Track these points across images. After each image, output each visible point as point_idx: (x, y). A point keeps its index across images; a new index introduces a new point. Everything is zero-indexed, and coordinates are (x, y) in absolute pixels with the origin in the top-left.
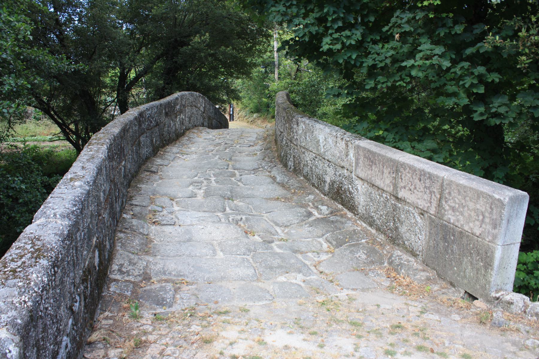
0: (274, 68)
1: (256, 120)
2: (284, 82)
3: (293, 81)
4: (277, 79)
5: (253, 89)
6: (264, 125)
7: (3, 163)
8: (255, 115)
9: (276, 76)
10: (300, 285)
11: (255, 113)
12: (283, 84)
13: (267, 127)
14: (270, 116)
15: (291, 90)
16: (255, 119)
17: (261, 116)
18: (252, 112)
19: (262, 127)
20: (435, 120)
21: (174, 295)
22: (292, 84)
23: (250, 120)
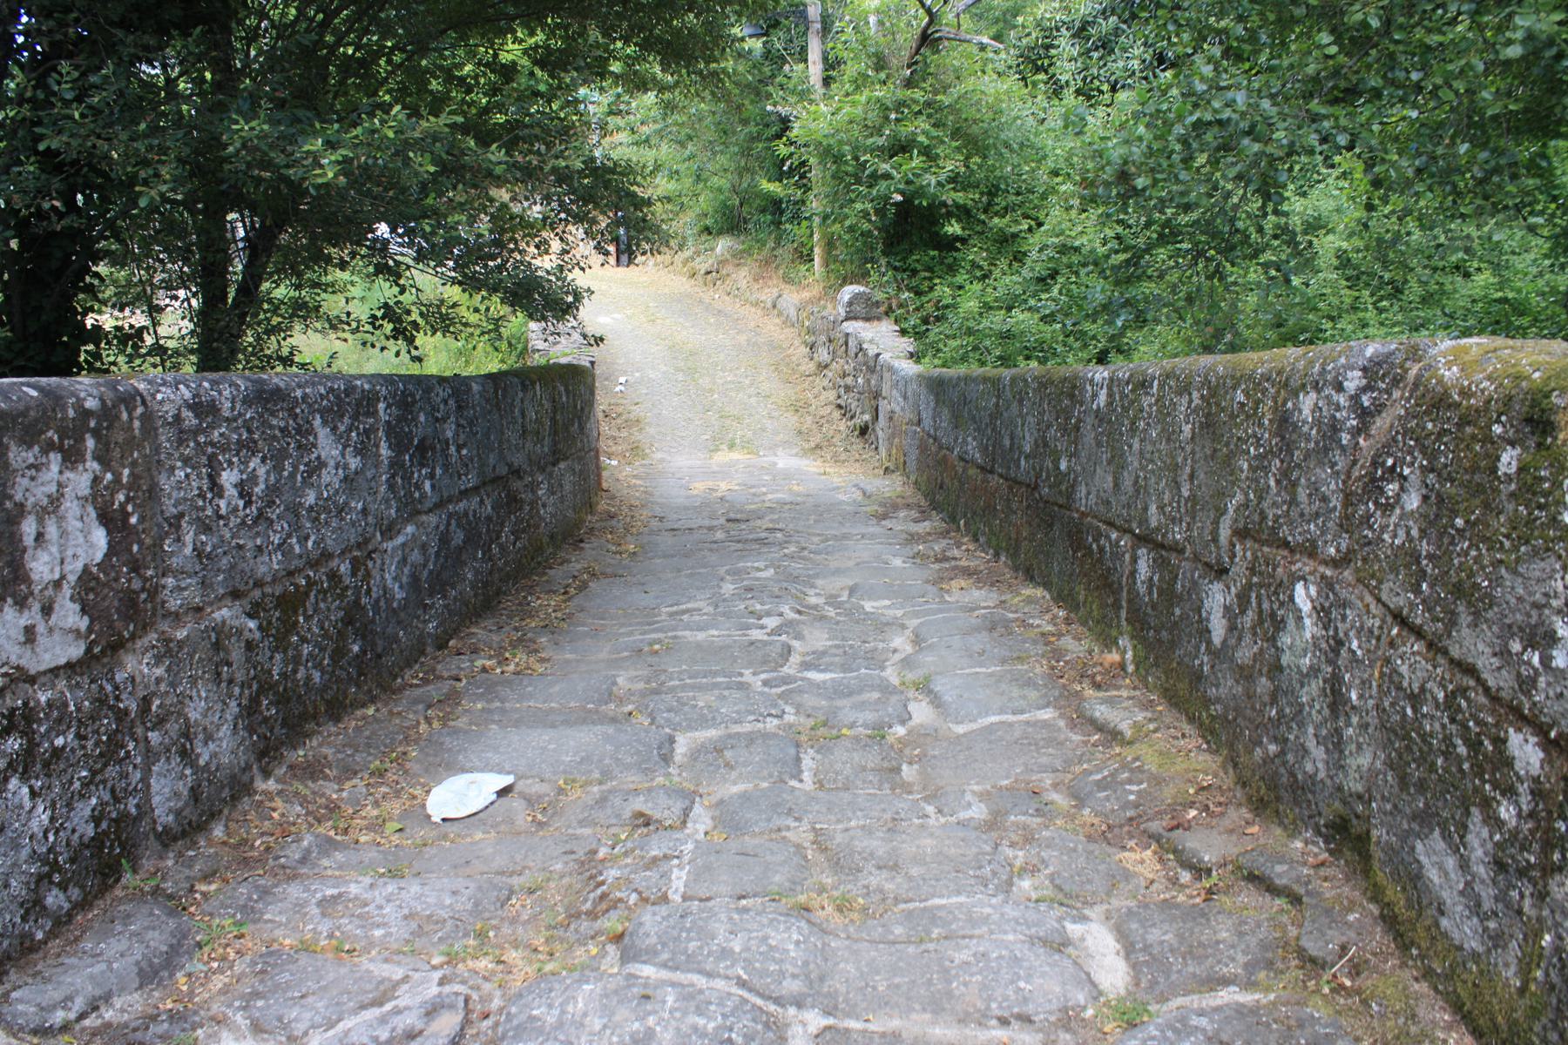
0: (805, 33)
1: (729, 269)
2: (863, 99)
3: (903, 94)
4: (819, 89)
5: (711, 135)
6: (767, 295)
7: (1563, 129)
8: (723, 245)
9: (815, 70)
10: (828, 1028)
11: (720, 233)
12: (859, 111)
13: (782, 303)
14: (785, 253)
15: (894, 137)
16: (722, 262)
17: (748, 252)
18: (707, 230)
19: (756, 304)
20: (137, 806)
21: (1452, 661)
22: (900, 105)
23: (702, 264)
